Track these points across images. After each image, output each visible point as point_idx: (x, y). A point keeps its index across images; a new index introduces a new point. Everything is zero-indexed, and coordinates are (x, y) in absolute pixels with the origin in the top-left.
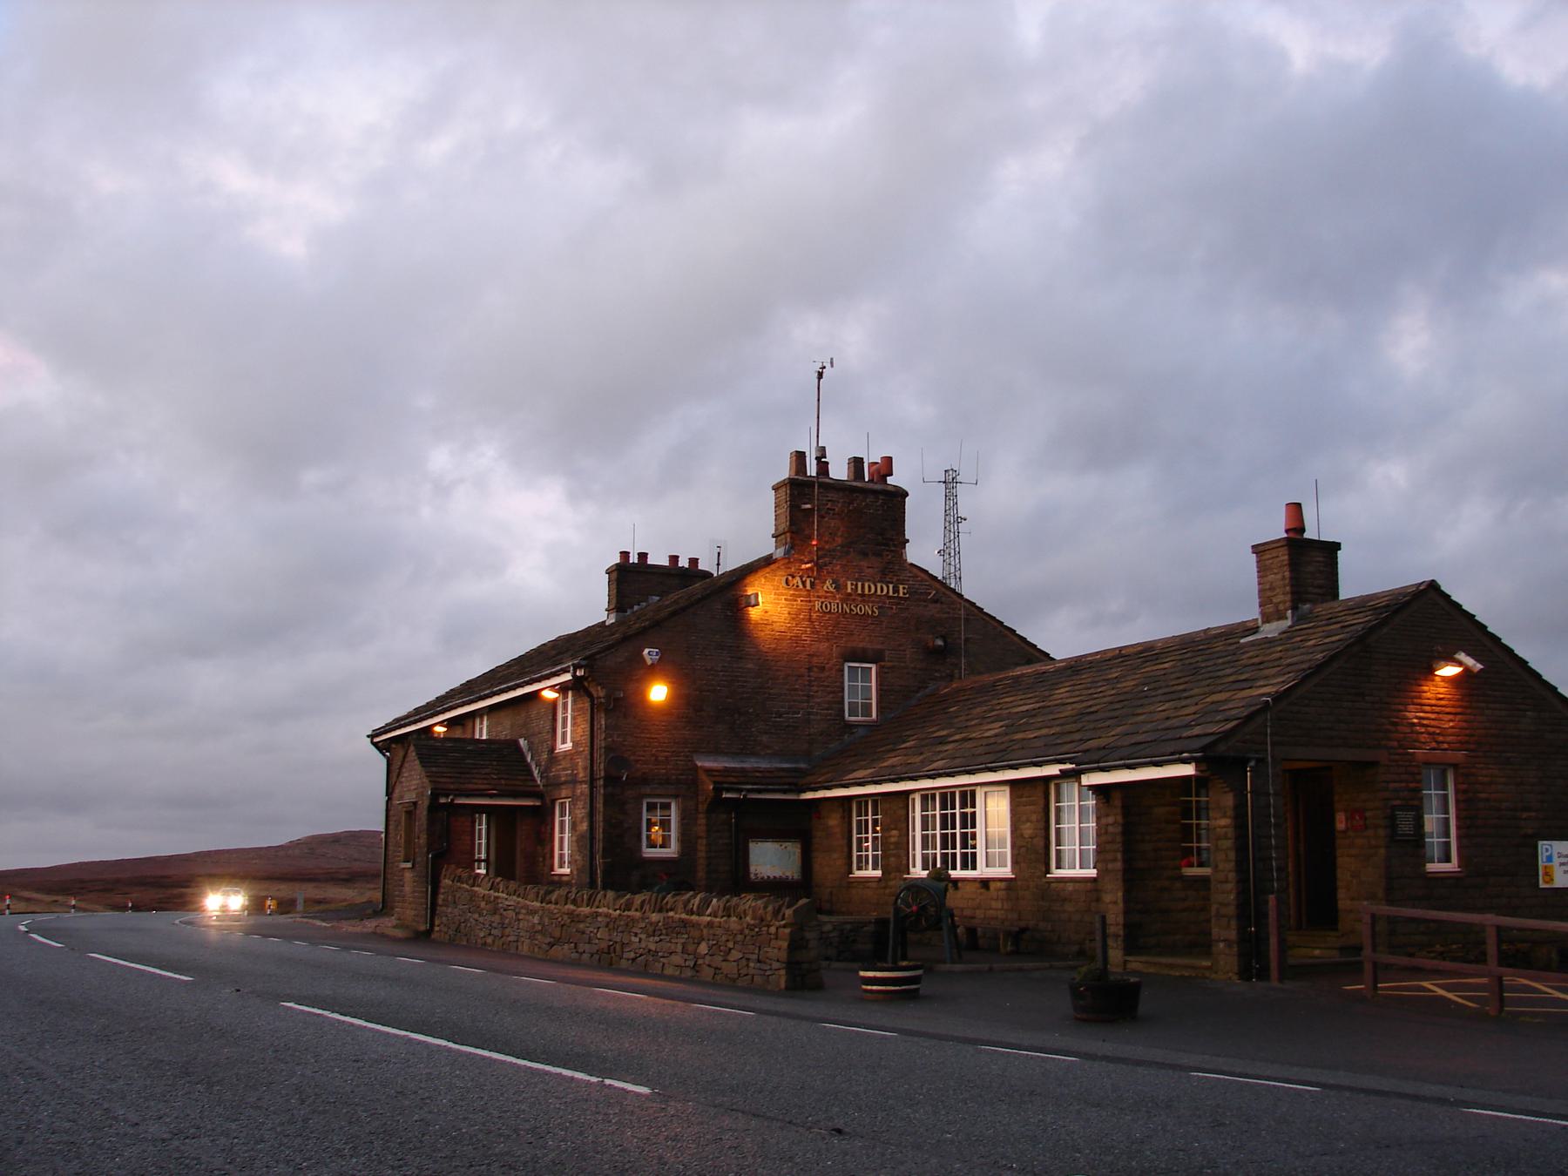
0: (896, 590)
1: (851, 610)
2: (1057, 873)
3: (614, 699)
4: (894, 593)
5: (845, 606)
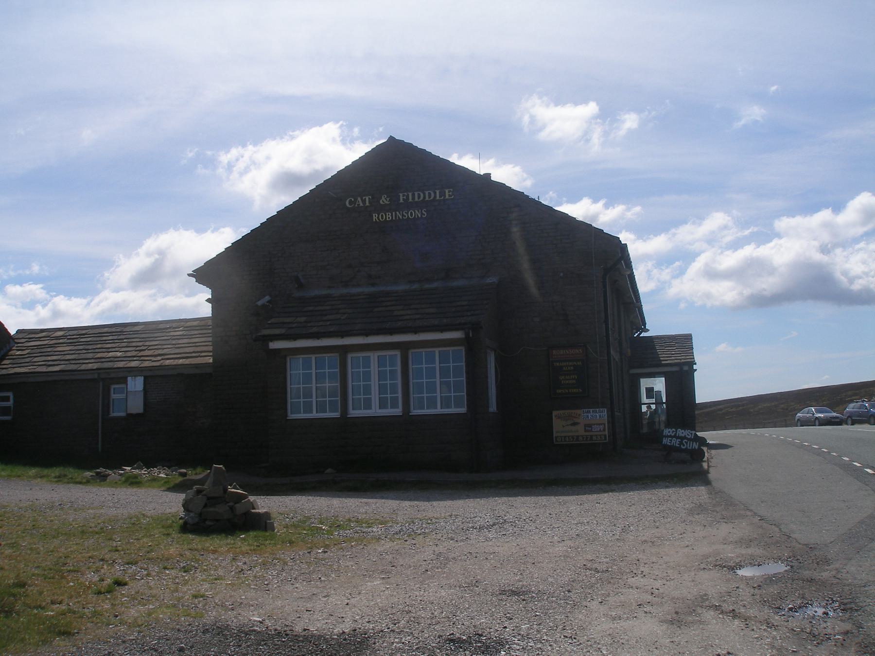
1: (403, 215)
5: (397, 213)
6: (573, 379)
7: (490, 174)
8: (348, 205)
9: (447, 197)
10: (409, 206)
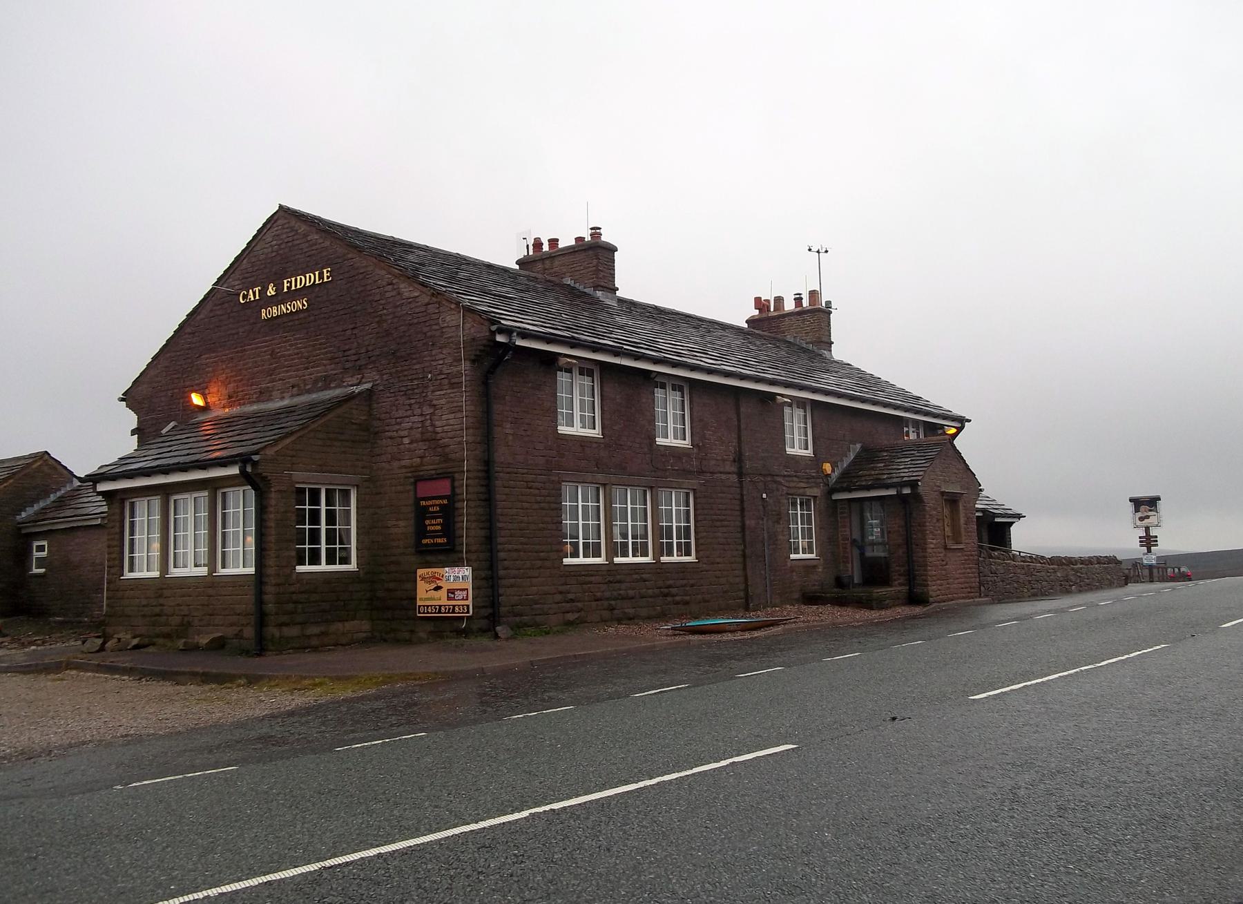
0: (321, 277)
1: (287, 309)
2: (128, 575)
3: (683, 386)
4: (319, 281)
6: (438, 524)
7: (617, 251)
8: (242, 302)
9: (325, 280)
10: (294, 295)
